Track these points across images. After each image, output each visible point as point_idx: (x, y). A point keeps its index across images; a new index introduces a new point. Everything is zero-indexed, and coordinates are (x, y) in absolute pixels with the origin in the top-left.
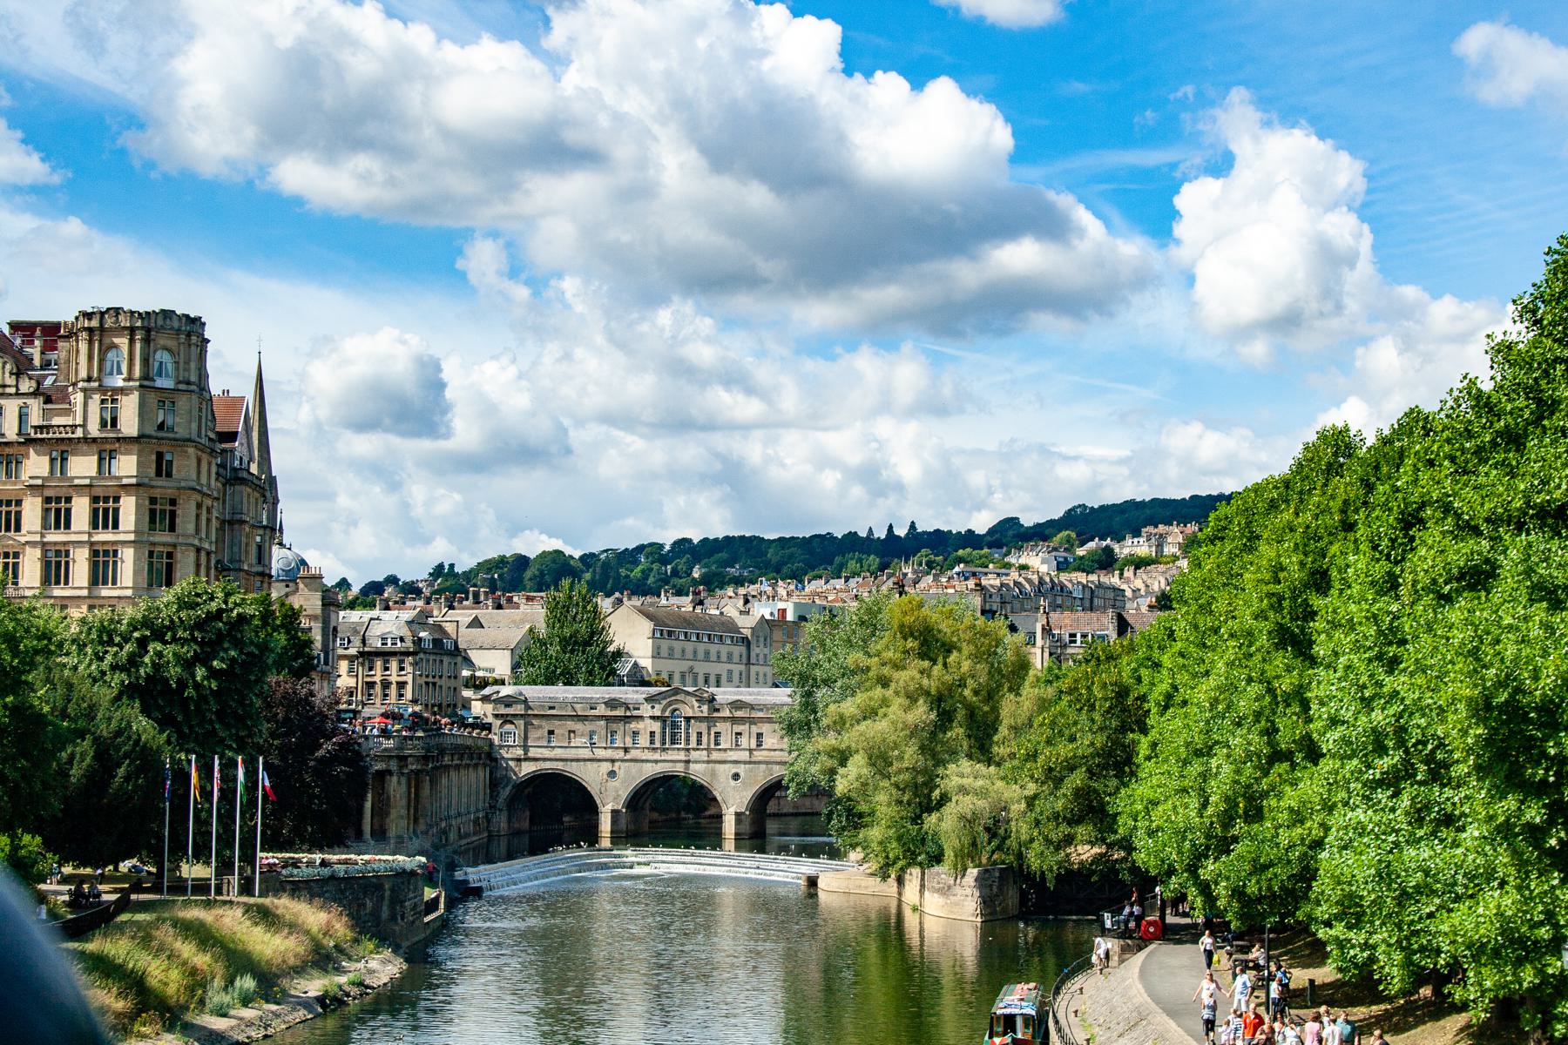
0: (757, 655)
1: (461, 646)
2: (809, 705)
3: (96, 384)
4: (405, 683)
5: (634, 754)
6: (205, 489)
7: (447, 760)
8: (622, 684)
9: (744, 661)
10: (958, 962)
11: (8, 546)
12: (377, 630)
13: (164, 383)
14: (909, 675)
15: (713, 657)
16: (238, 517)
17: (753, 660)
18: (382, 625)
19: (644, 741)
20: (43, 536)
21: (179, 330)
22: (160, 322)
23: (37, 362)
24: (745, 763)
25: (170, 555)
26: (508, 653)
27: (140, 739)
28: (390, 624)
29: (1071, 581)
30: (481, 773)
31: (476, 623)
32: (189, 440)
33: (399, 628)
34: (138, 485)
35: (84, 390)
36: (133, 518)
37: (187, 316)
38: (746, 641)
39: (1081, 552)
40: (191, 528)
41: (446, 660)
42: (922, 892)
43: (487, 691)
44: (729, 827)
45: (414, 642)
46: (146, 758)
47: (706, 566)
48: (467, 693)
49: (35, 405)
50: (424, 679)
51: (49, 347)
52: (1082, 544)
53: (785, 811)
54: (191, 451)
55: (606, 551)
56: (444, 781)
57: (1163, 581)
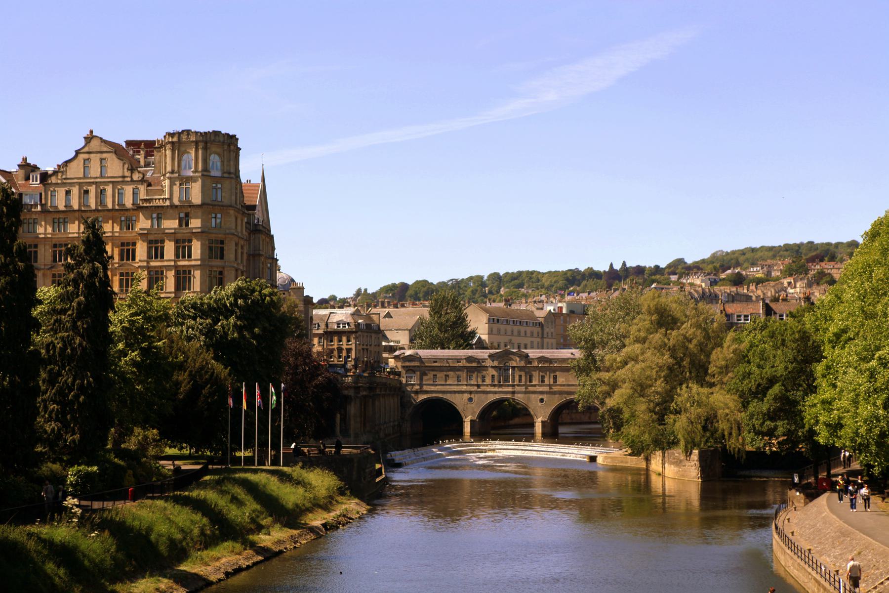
0: (548, 333)
1: (382, 328)
2: (590, 356)
3: (176, 175)
4: (351, 349)
5: (483, 388)
6: (240, 234)
7: (378, 392)
8: (471, 348)
9: (540, 336)
10: (688, 503)
11: (128, 269)
12: (334, 319)
13: (216, 173)
14: (657, 337)
15: (523, 333)
16: (257, 252)
17: (545, 336)
18: (337, 317)
19: (488, 381)
20: (148, 262)
21: (223, 142)
22: (212, 138)
23: (142, 163)
24: (547, 393)
25: (221, 273)
26: (407, 332)
27: (214, 372)
28: (342, 315)
29: (721, 291)
30: (396, 399)
31: (388, 315)
32: (231, 206)
33: (347, 318)
34: (202, 232)
35: (170, 178)
36: (199, 251)
37: (228, 135)
38: (540, 324)
39: (723, 276)
40: (232, 256)
41: (374, 336)
42: (663, 464)
43: (397, 353)
44: (538, 429)
45: (355, 325)
46: (215, 380)
47: (508, 287)
48: (385, 355)
49: (142, 189)
50: (361, 347)
51: (148, 154)
52: (724, 271)
53: (565, 421)
54: (232, 212)
55: (452, 280)
56: (377, 403)
57: (773, 291)
